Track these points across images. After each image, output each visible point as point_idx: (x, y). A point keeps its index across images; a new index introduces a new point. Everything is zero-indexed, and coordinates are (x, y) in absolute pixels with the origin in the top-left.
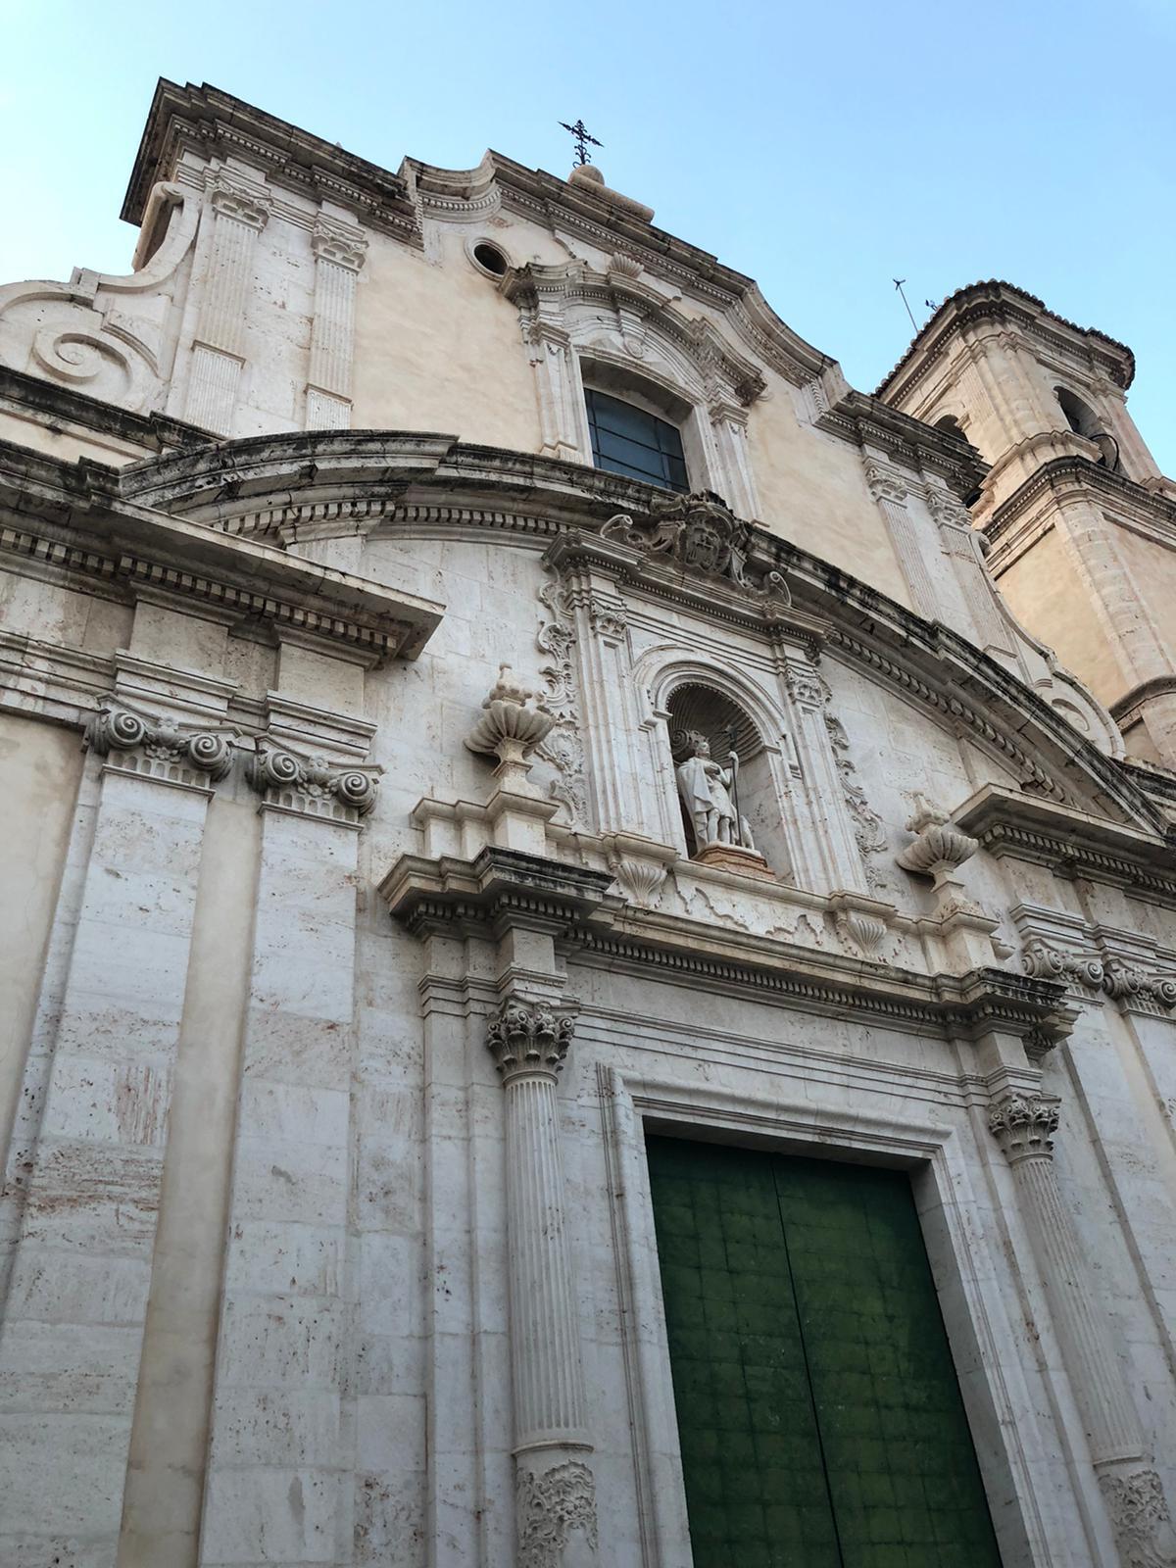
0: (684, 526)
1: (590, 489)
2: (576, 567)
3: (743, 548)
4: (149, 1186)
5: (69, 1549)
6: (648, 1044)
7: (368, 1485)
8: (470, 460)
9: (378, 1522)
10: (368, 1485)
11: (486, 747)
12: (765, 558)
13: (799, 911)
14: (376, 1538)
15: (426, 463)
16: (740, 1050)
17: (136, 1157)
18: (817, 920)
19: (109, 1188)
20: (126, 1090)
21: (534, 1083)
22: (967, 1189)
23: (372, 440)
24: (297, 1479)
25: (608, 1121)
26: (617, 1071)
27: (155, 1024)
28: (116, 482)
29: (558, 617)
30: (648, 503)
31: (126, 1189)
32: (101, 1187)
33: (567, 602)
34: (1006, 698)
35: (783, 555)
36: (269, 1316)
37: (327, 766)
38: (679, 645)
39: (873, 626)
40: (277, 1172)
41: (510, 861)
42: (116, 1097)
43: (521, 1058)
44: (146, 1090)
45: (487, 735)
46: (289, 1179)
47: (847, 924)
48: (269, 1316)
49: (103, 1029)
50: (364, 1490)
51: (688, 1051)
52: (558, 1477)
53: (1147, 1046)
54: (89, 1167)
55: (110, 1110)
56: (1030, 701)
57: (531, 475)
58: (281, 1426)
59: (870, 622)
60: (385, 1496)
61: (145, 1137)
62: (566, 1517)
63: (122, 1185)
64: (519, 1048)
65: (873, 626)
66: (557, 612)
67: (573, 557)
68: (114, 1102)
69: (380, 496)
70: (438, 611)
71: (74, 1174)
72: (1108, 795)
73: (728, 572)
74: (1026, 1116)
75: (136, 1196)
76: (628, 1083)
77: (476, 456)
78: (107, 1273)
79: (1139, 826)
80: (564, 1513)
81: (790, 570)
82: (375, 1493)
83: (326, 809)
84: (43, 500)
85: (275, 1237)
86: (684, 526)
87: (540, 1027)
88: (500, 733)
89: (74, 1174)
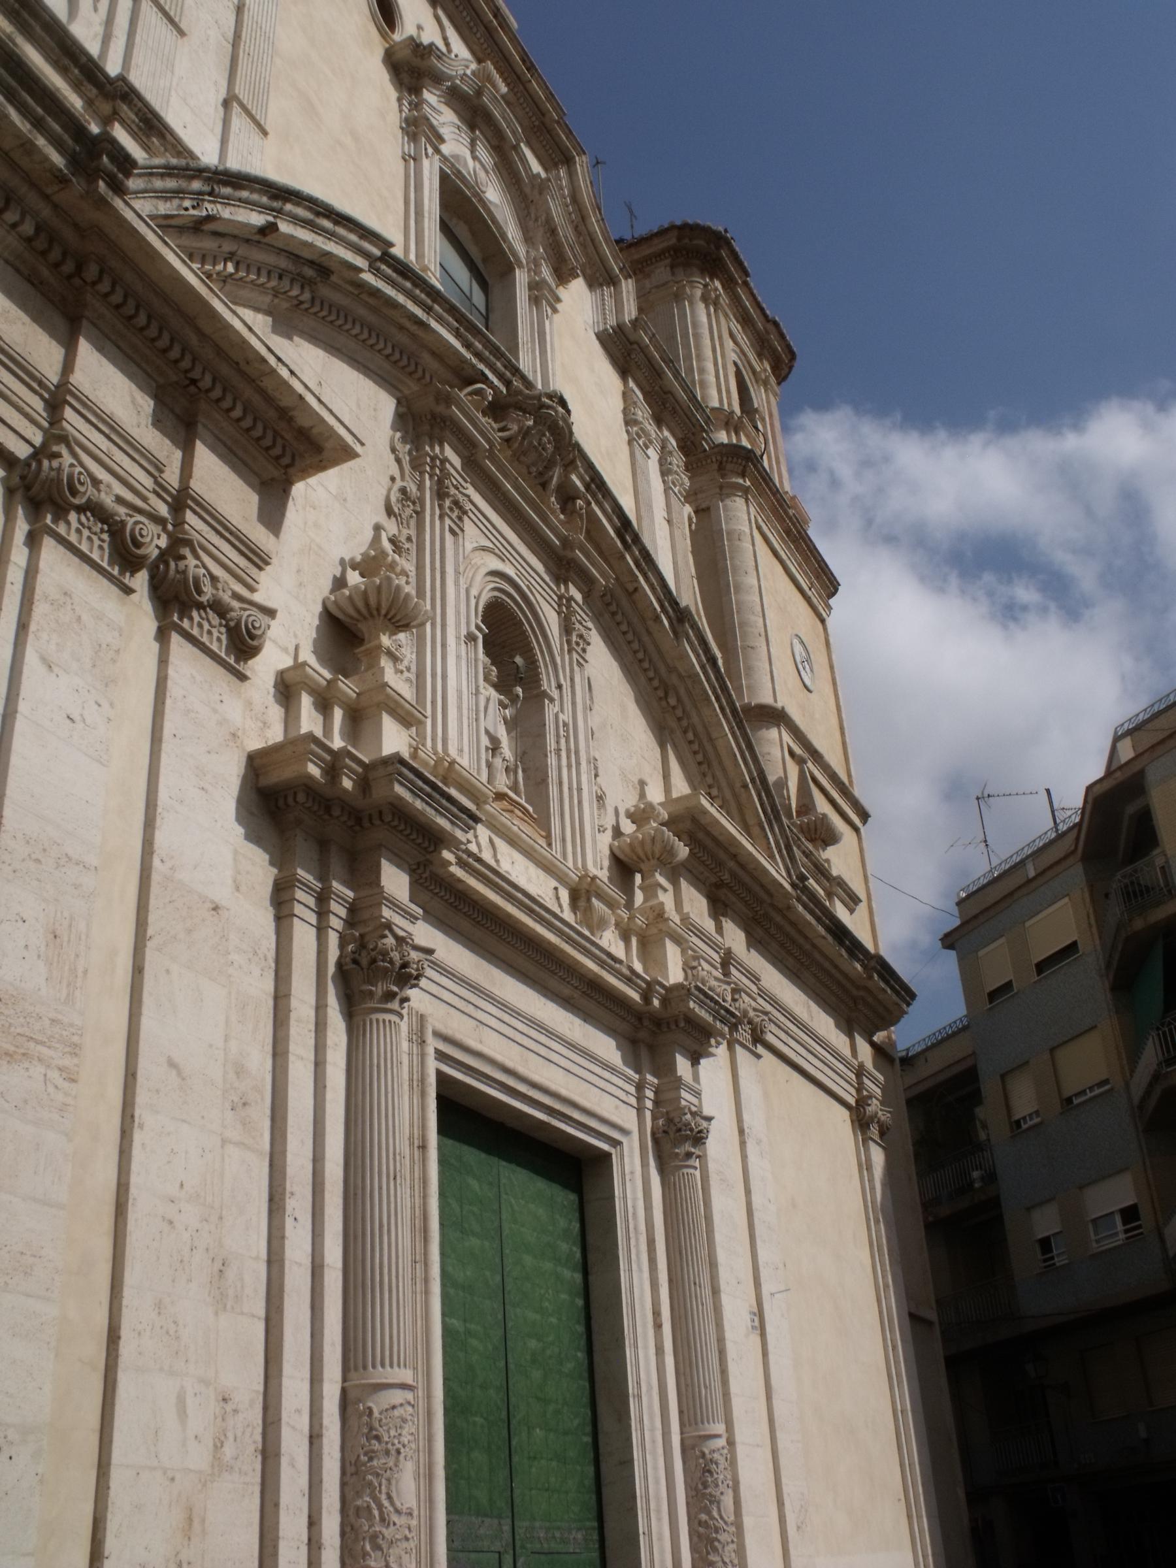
0: (531, 423)
1: (468, 346)
2: (432, 426)
3: (566, 466)
4: (71, 1054)
5: (9, 1438)
6: (446, 996)
7: (224, 1400)
8: (389, 271)
9: (230, 1435)
10: (224, 1400)
11: (351, 617)
12: (578, 483)
13: (554, 883)
14: (229, 1450)
15: (360, 262)
16: (506, 1018)
17: (60, 1017)
18: (564, 895)
19: (39, 1047)
20: (52, 936)
21: (384, 1021)
22: (635, 1184)
23: (327, 217)
24: (182, 1387)
25: (415, 1069)
26: (430, 1020)
27: (77, 864)
28: (128, 175)
29: (407, 477)
30: (508, 384)
31: (51, 1053)
32: (32, 1045)
33: (416, 465)
34: (716, 705)
35: (593, 486)
36: (164, 1218)
37: (230, 593)
38: (497, 551)
39: (636, 590)
40: (172, 1064)
41: (411, 776)
42: (44, 943)
43: (380, 992)
44: (69, 941)
45: (360, 604)
46: (179, 1073)
47: (589, 907)
48: (164, 1218)
49: (33, 856)
50: (222, 1404)
51: (470, 1009)
52: (396, 1413)
53: (743, 1072)
54: (22, 1020)
55: (39, 956)
56: (733, 716)
57: (428, 310)
58: (172, 1332)
59: (635, 585)
60: (236, 1411)
61: (68, 995)
62: (402, 1450)
63: (49, 1047)
64: (369, 977)
65: (636, 590)
66: (407, 472)
67: (434, 416)
68: (43, 948)
69: (303, 277)
70: (358, 448)
71: (10, 1025)
72: (763, 829)
73: (544, 485)
74: (691, 1130)
75: (61, 1063)
76: (437, 1034)
77: (395, 270)
78: (38, 1144)
79: (777, 864)
80: (400, 1446)
81: (593, 504)
82: (229, 1407)
83: (218, 641)
84: (46, 159)
85: (169, 1134)
86: (531, 423)
87: (405, 965)
88: (378, 610)
89: (10, 1025)
